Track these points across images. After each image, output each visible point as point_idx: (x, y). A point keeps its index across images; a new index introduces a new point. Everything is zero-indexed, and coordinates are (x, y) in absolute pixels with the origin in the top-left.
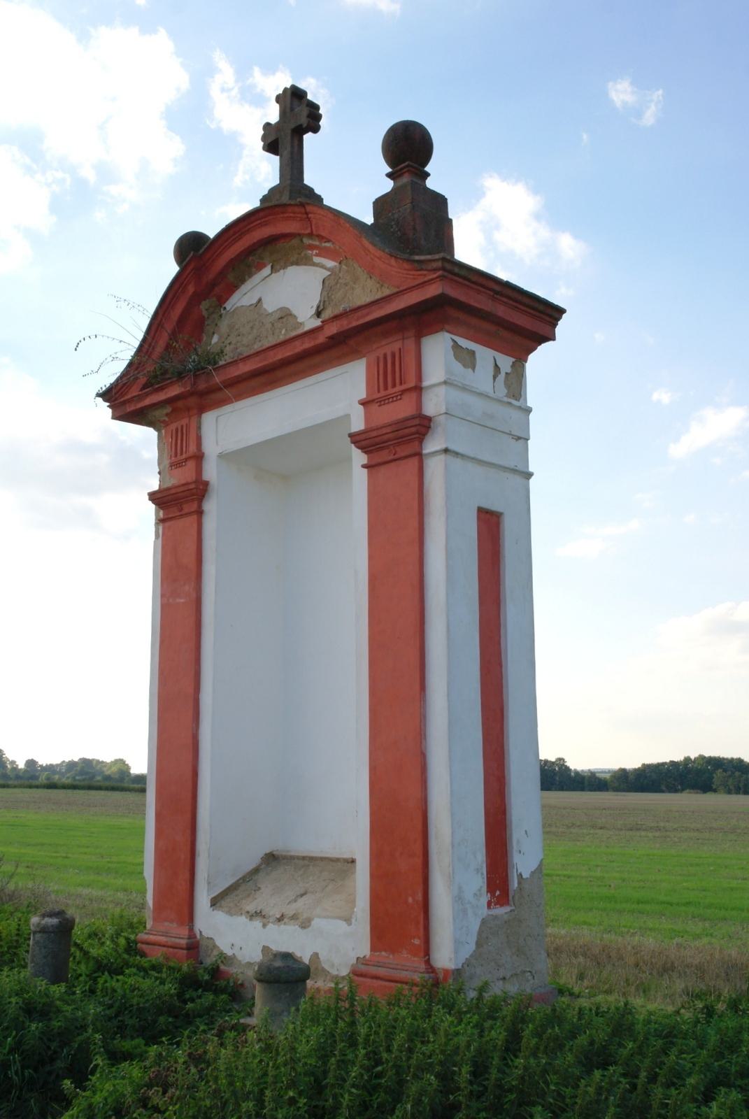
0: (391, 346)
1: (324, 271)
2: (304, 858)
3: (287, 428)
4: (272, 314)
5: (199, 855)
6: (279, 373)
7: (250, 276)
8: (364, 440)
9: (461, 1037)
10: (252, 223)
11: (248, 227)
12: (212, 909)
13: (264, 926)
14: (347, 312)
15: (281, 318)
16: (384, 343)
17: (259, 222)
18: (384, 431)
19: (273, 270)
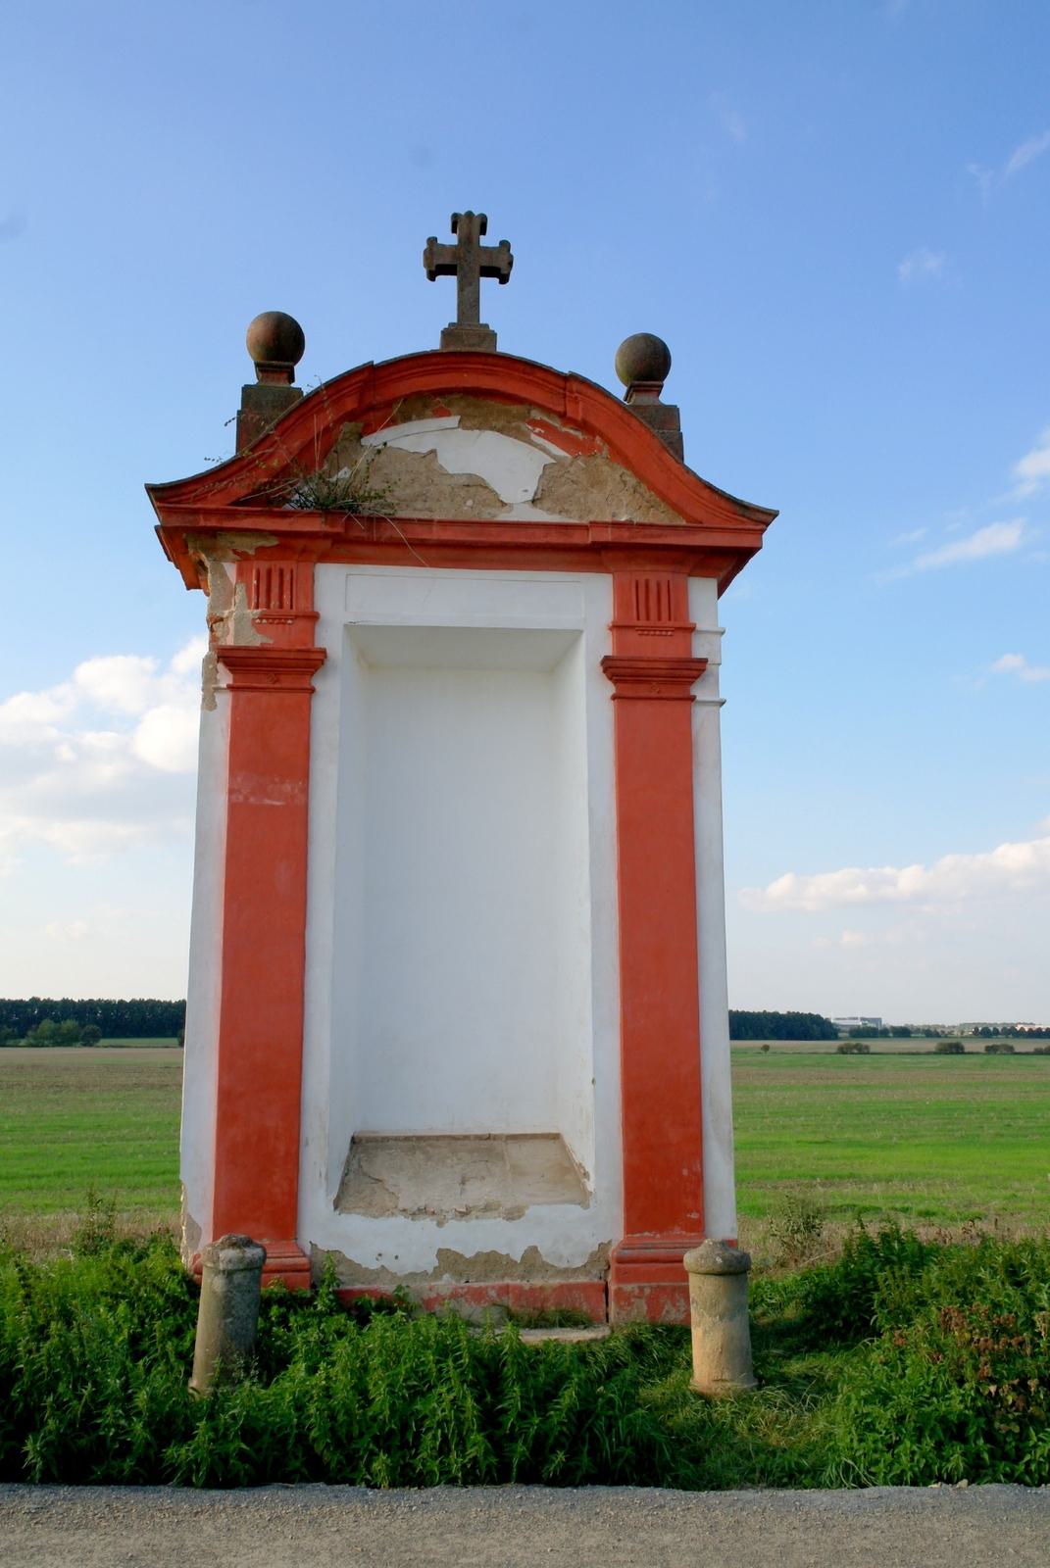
0: (656, 575)
1: (549, 458)
2: (407, 1139)
4: (452, 476)
5: (307, 1144)
6: (481, 554)
7: (421, 416)
9: (435, 1328)
11: (461, 366)
12: (338, 1212)
13: (440, 1224)
15: (468, 486)
17: (481, 366)
18: (657, 665)
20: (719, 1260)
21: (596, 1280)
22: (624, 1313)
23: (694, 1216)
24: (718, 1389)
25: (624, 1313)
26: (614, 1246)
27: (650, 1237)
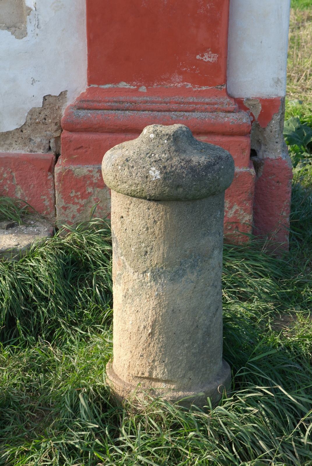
20: (155, 173)
21: (40, 152)
22: (75, 208)
23: (209, 58)
24: (137, 397)
25: (75, 208)
26: (71, 100)
27: (128, 91)
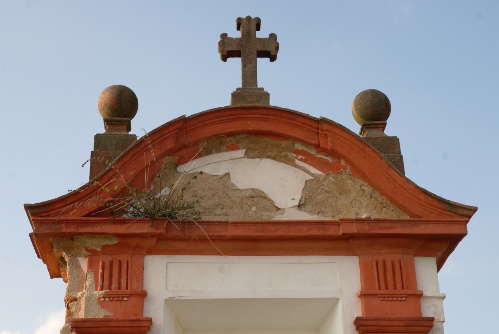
0: (391, 256)
3: (264, 293)
4: (241, 190)
8: (374, 326)
10: (252, 114)
14: (371, 220)
15: (252, 197)
16: (384, 251)
18: (396, 323)
19: (247, 155)
